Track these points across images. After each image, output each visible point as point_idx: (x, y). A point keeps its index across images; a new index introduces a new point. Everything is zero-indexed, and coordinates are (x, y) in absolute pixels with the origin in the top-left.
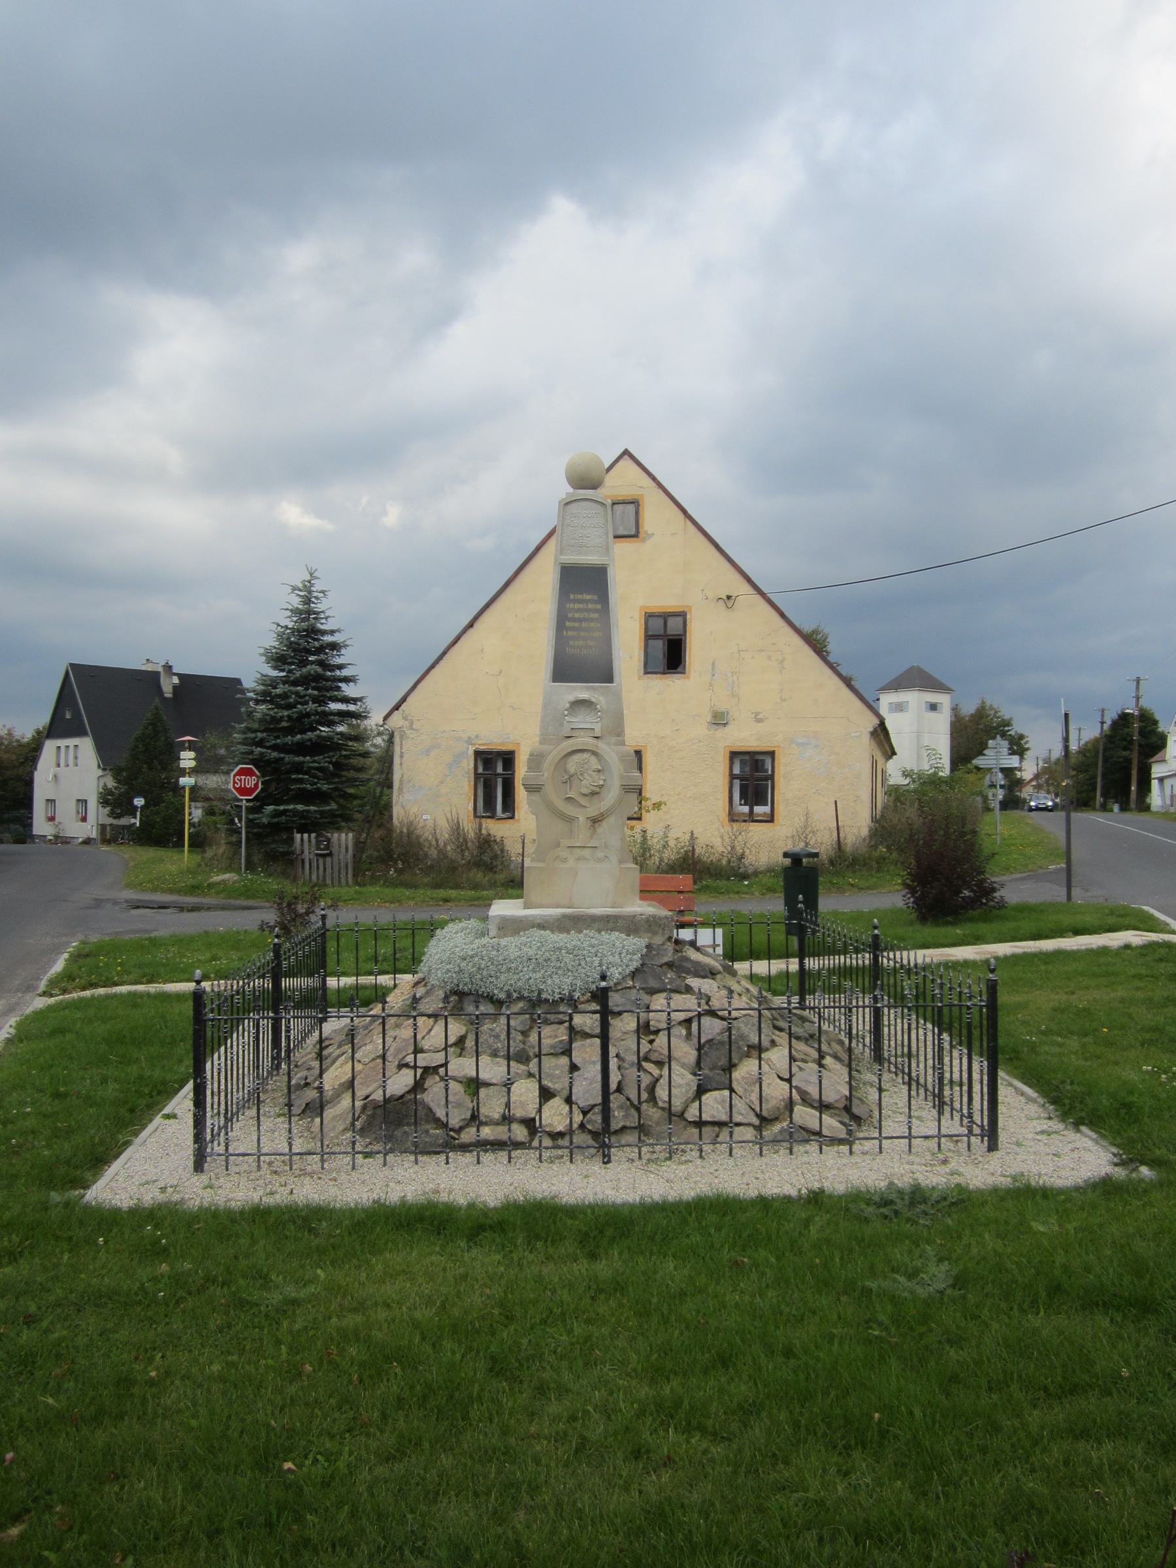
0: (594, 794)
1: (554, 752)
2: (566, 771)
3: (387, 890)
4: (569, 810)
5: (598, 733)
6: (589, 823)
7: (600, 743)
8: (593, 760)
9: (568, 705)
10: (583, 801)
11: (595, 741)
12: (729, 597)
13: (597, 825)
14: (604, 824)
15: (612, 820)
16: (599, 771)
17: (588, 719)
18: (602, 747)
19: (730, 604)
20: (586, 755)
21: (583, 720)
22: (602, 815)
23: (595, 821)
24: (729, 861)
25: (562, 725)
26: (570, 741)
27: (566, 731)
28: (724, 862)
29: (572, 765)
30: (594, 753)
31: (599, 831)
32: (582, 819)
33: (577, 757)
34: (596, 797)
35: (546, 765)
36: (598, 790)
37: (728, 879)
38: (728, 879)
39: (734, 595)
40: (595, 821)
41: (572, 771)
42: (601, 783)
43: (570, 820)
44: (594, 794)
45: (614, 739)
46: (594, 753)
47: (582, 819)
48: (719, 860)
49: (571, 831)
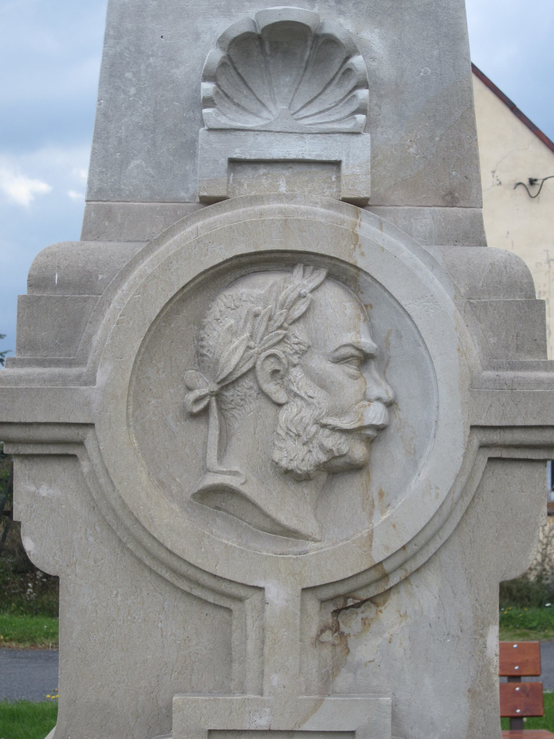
0: (337, 470)
1: (145, 266)
2: (200, 359)
3: (19, 620)
4: (219, 549)
5: (357, 176)
6: (317, 616)
7: (367, 225)
8: (335, 302)
9: (215, 55)
10: (288, 507)
11: (347, 215)
12: (532, 182)
13: (352, 624)
14: (389, 615)
15: (424, 597)
16: (364, 359)
17: (311, 119)
18: (378, 244)
19: (534, 191)
20: (299, 281)
21: (283, 121)
22: (379, 572)
23: (346, 603)
24: (540, 578)
25: (189, 149)
26: (218, 217)
27: (208, 172)
28: (532, 578)
29: (234, 323)
30: (343, 273)
31: (365, 650)
32: (279, 595)
33: (257, 291)
34: (349, 490)
35: (101, 332)
36: (358, 451)
37: (541, 605)
38: (541, 605)
39: (539, 175)
40: (346, 603)
41: (231, 354)
42: (375, 414)
43: (220, 597)
44: (337, 470)
45: (429, 217)
46: (343, 273)
47: (279, 595)
48: (525, 576)
49: (227, 653)
